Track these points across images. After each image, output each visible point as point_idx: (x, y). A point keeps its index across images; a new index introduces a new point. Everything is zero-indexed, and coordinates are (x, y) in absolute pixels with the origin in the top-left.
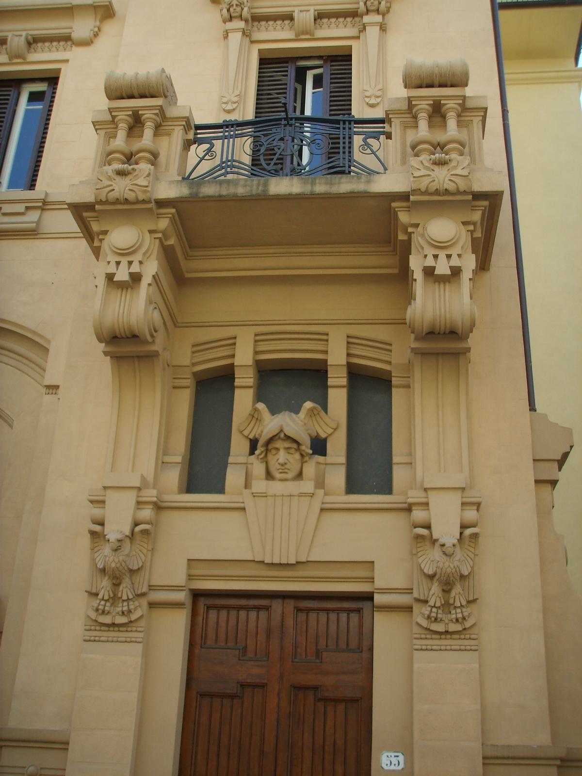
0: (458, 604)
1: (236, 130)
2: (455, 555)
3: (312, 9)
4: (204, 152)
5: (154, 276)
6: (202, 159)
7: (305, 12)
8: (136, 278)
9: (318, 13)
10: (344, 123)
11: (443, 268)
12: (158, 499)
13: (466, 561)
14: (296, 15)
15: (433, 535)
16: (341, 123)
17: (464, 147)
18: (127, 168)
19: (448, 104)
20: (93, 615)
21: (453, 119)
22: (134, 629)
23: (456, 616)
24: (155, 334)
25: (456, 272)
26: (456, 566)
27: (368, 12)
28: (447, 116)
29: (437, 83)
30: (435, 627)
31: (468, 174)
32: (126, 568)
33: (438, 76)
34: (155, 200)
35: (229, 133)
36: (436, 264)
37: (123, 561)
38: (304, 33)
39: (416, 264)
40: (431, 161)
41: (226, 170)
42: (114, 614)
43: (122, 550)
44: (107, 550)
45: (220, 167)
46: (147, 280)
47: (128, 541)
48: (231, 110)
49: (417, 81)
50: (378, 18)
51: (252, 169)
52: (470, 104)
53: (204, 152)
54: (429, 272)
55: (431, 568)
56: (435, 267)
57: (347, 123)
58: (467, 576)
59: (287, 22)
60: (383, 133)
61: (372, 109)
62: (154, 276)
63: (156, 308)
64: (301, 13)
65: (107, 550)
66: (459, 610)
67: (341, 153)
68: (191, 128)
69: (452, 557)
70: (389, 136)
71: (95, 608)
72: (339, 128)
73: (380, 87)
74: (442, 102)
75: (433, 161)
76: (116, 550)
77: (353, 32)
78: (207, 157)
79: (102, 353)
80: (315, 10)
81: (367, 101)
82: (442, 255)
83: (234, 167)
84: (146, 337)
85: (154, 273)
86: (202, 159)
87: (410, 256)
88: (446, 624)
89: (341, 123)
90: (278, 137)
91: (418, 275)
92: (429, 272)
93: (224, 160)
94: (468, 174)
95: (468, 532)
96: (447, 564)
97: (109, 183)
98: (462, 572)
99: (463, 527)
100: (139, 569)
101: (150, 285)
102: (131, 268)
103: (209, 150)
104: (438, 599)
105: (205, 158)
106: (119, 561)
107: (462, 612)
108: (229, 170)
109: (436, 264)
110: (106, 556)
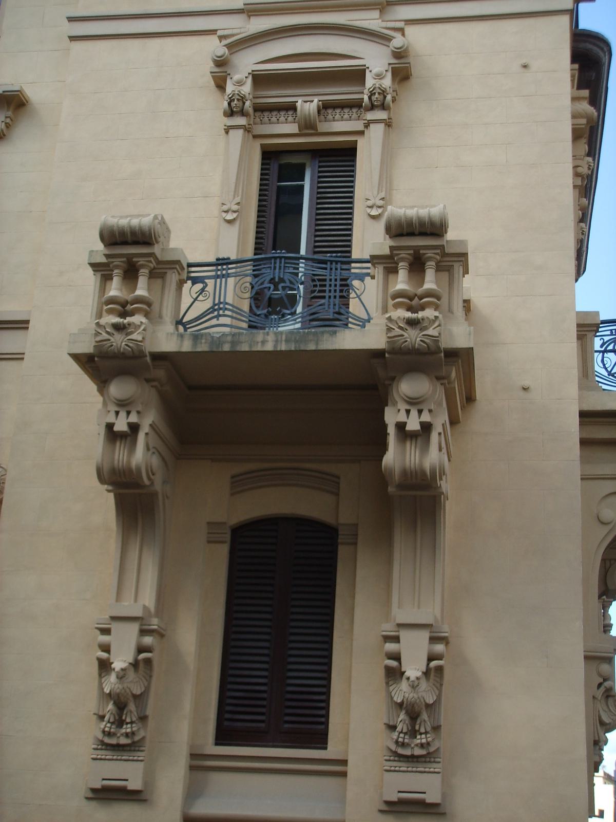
0: (422, 730)
1: (229, 269)
2: (420, 686)
3: (316, 101)
4: (196, 293)
5: (151, 425)
6: (196, 299)
7: (309, 103)
8: (134, 428)
9: (322, 103)
10: (331, 264)
11: (413, 425)
12: (159, 626)
13: (432, 691)
14: (299, 105)
15: (402, 668)
16: (329, 263)
17: (439, 298)
18: (123, 322)
19: (428, 253)
20: (100, 736)
21: (431, 269)
22: (137, 748)
23: (421, 741)
24: (152, 477)
25: (426, 428)
26: (420, 696)
27: (372, 107)
28: (426, 265)
29: (417, 232)
30: (401, 751)
31: (438, 335)
32: (130, 694)
33: (417, 224)
34: (150, 353)
35: (222, 272)
36: (408, 418)
37: (127, 687)
38: (308, 126)
39: (391, 417)
40: (405, 320)
41: (218, 313)
42: (118, 735)
43: (126, 677)
44: (113, 678)
45: (212, 309)
46: (145, 429)
47: (132, 669)
48: (232, 219)
49: (400, 230)
50: (382, 115)
51: (254, 266)
52: (448, 250)
53: (196, 293)
54: (401, 427)
55: (399, 698)
56: (406, 423)
57: (334, 263)
58: (433, 704)
59: (290, 113)
60: (368, 274)
61: (372, 220)
62: (151, 425)
63: (154, 453)
64: (305, 104)
65: (113, 678)
66: (423, 736)
67: (338, 280)
68: (184, 269)
69: (417, 688)
70: (373, 277)
71: (101, 730)
72: (326, 269)
73: (383, 195)
74: (421, 252)
75: (406, 320)
76: (121, 678)
77: (358, 126)
78: (201, 298)
79: (88, 265)
80: (320, 101)
81: (368, 212)
82: (414, 413)
83: (226, 309)
84: (141, 478)
85: (151, 422)
86: (196, 299)
87: (386, 408)
88: (412, 748)
89: (329, 263)
90: (268, 279)
91: (391, 430)
92: (401, 427)
93: (217, 302)
94: (438, 335)
95: (434, 664)
96: (411, 695)
97: (107, 337)
98: (427, 701)
99: (430, 659)
100: (142, 693)
101: (147, 434)
102: (129, 418)
103: (203, 290)
104: (405, 725)
105: (198, 299)
106: (123, 688)
107: (426, 738)
108: (221, 312)
109: (408, 418)
110: (111, 683)
